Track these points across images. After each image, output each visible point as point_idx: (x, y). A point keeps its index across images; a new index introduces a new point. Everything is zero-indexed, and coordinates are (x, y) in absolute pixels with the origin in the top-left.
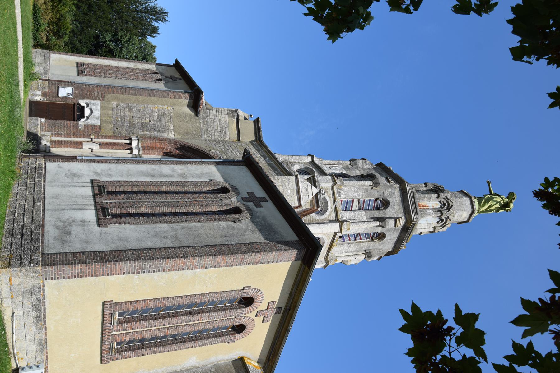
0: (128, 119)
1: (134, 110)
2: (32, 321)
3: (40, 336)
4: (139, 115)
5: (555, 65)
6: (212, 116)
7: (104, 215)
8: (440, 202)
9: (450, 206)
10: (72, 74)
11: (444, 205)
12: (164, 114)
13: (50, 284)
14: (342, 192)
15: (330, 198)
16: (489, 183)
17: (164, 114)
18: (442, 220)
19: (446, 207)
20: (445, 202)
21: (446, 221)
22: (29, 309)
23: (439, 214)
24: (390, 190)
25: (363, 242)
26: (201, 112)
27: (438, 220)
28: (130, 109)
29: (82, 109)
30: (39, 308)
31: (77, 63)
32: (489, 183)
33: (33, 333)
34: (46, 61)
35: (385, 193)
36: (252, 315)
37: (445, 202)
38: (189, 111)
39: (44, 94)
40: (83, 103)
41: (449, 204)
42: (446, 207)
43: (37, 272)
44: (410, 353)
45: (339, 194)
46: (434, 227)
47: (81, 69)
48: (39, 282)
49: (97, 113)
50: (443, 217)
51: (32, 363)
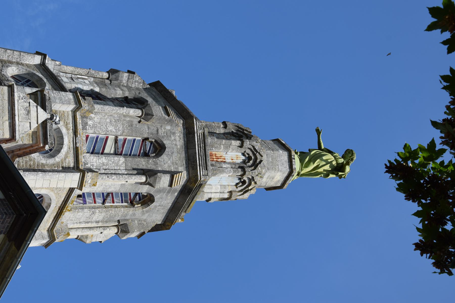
9: (258, 161)
11: (249, 158)
14: (90, 122)
15: (68, 129)
18: (244, 182)
20: (251, 154)
25: (116, 207)
37: (251, 154)
41: (256, 158)
45: (85, 125)
46: (231, 192)
50: (245, 178)
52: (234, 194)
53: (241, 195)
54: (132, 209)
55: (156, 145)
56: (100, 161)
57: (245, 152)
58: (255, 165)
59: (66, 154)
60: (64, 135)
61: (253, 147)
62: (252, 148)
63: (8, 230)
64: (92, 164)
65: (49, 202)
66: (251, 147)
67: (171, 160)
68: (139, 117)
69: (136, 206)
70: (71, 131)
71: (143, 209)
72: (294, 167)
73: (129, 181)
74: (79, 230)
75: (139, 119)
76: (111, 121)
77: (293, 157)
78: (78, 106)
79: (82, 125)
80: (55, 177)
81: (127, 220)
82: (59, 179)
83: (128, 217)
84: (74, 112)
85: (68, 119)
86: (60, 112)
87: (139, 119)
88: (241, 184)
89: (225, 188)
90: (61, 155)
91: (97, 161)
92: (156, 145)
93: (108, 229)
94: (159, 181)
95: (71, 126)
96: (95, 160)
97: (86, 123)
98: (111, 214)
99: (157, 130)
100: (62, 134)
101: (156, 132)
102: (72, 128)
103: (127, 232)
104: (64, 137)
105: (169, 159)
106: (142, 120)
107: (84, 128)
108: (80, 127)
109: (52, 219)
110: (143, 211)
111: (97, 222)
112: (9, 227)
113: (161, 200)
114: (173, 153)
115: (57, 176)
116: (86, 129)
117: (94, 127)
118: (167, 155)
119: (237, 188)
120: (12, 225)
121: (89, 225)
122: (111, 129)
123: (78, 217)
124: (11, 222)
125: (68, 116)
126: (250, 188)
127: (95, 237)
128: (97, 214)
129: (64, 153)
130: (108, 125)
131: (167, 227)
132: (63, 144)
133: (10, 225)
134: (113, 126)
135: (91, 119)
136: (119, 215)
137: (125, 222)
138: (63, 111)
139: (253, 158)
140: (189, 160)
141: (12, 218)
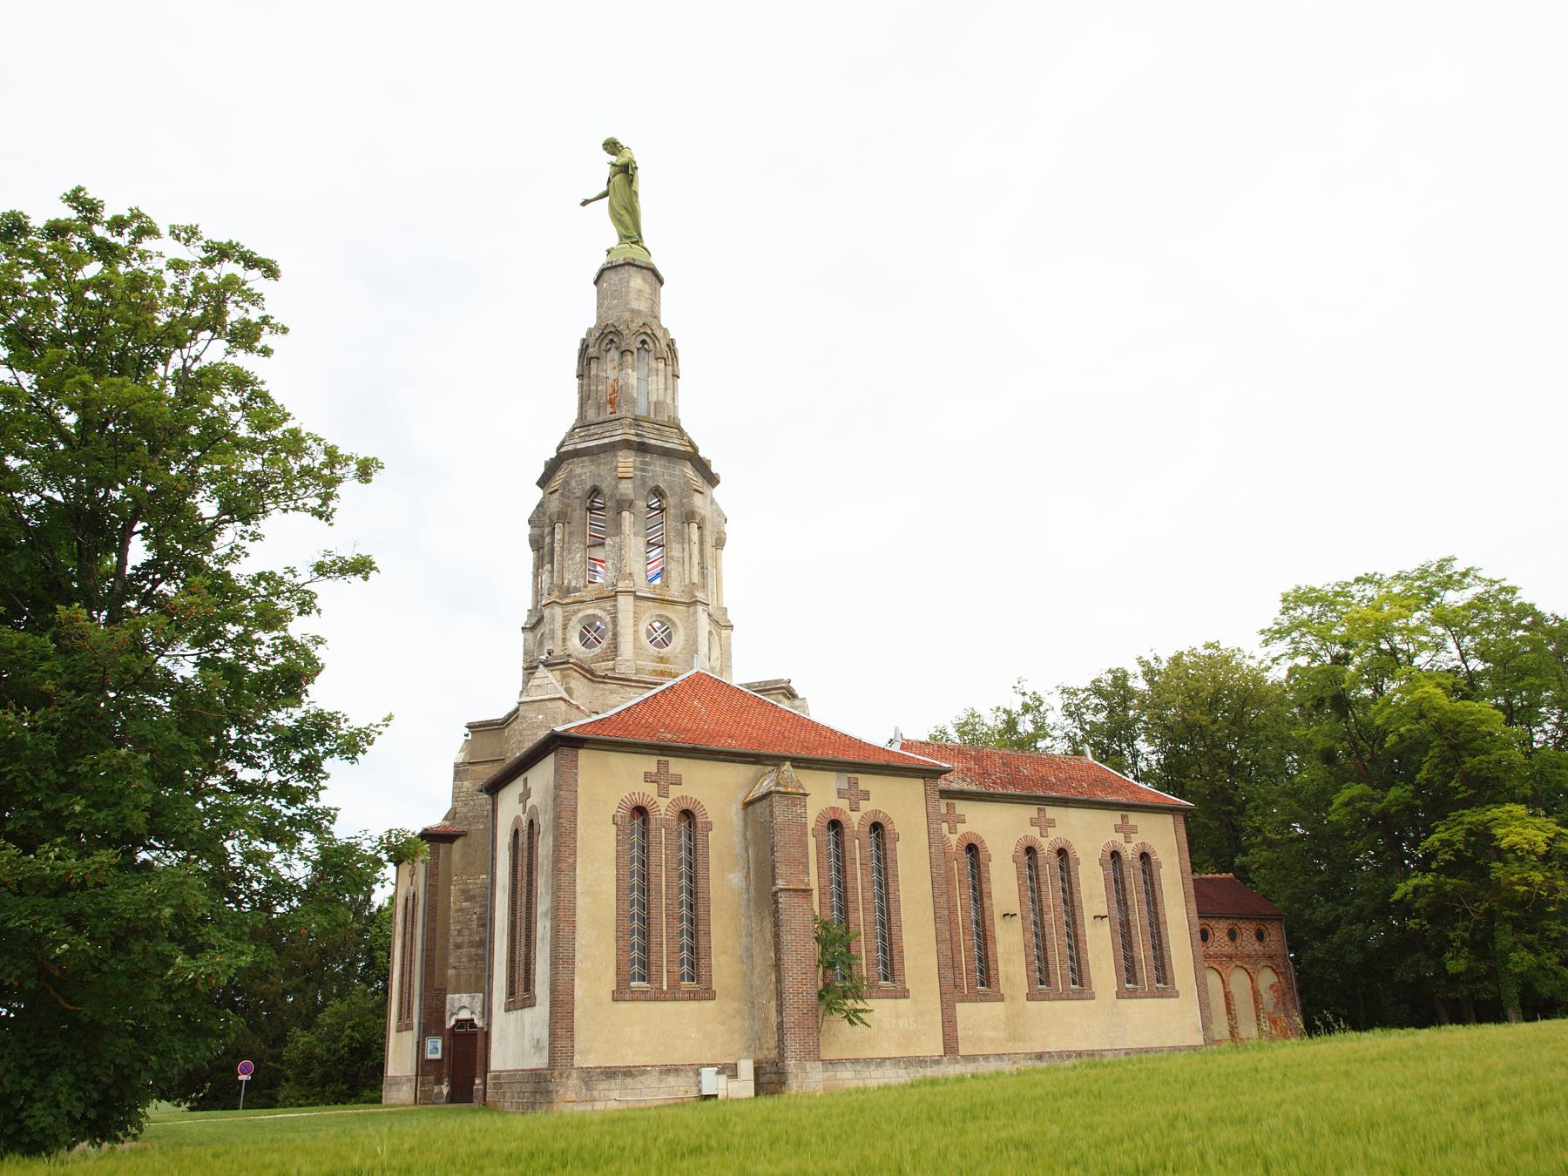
0: (473, 950)
1: (459, 940)
2: (629, 1080)
3: (655, 1074)
4: (466, 932)
5: (276, 545)
6: (465, 810)
7: (529, 1002)
10: (410, 1038)
11: (612, 341)
12: (464, 891)
13: (579, 1061)
16: (585, 203)
17: (464, 891)
22: (613, 1084)
26: (459, 828)
28: (458, 946)
29: (460, 1023)
30: (610, 1073)
31: (507, 1010)
32: (585, 203)
33: (651, 1080)
34: (397, 1081)
36: (663, 804)
38: (458, 844)
39: (439, 1082)
40: (450, 1023)
43: (561, 1075)
47: (404, 1027)
48: (574, 1074)
49: (465, 999)
51: (693, 1080)
95: (576, 607)
107: (577, 590)
117: (577, 578)
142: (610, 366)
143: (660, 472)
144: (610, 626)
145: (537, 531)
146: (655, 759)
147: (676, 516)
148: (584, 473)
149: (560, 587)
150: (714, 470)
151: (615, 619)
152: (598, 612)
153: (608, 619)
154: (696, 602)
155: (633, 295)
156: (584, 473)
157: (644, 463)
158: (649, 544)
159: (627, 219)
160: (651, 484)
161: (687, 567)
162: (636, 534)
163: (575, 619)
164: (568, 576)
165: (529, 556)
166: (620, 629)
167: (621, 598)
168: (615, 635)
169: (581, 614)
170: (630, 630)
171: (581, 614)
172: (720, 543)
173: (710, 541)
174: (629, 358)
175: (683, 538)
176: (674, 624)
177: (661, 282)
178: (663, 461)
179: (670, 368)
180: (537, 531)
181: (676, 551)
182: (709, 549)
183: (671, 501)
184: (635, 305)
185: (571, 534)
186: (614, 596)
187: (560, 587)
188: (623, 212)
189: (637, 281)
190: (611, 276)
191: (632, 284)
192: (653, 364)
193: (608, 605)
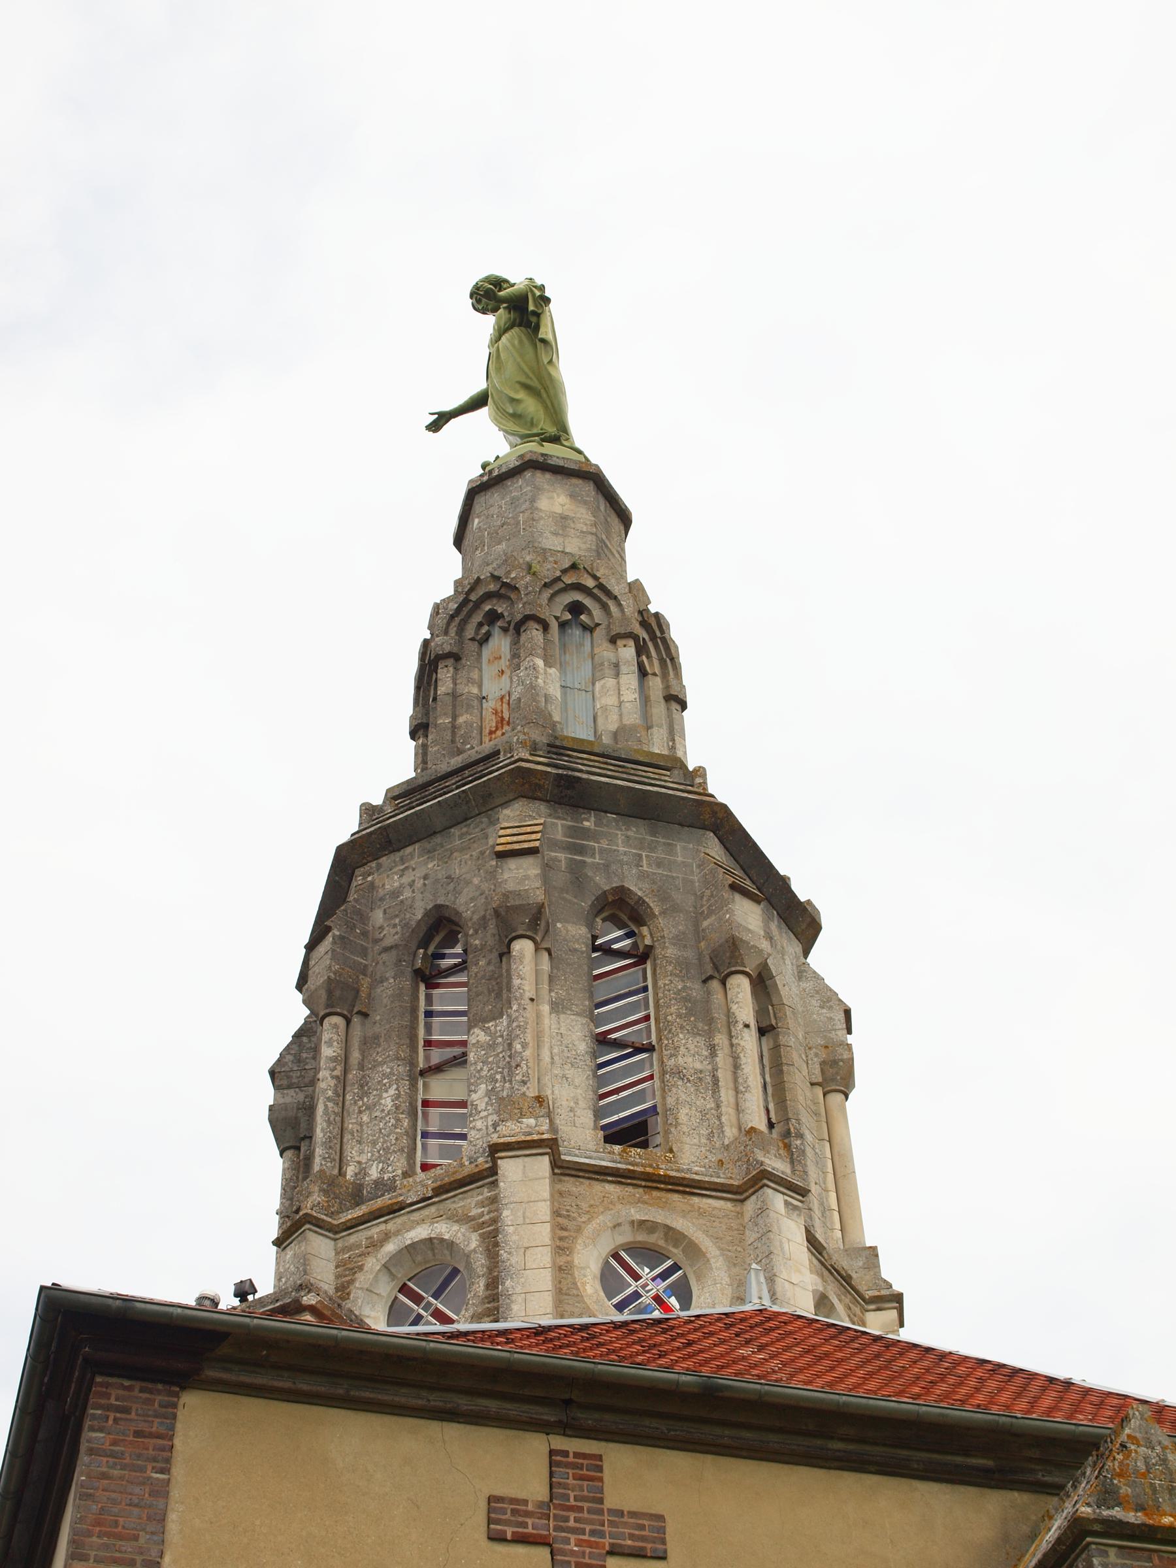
8: (487, 638)
9: (492, 587)
11: (493, 617)
14: (374, 1173)
15: (386, 1237)
16: (439, 422)
18: (576, 609)
19: (587, 602)
20: (478, 617)
21: (578, 587)
23: (534, 634)
24: (378, 917)
25: (657, 1006)
27: (577, 632)
32: (439, 422)
35: (388, 942)
37: (478, 617)
41: (488, 596)
42: (587, 602)
44: (368, 811)
45: (382, 1186)
46: (613, 640)
50: (557, 610)
52: (617, 629)
53: (620, 605)
54: (658, 951)
55: (437, 939)
56: (482, 1106)
57: (472, 639)
58: (506, 590)
59: (457, 1221)
60: (402, 1246)
61: (452, 617)
62: (457, 620)
63: (160, 1386)
64: (491, 1129)
65: (626, 1228)
66: (453, 624)
67: (468, 876)
68: (348, 1022)
69: (648, 942)
70: (391, 1226)
71: (654, 916)
72: (517, 463)
73: (528, 995)
74: (743, 1105)
75: (356, 1020)
76: (368, 1108)
77: (496, 473)
78: (307, 1226)
79: (383, 1195)
80: (515, 1238)
81: (700, 956)
82: (520, 1221)
83: (690, 954)
84: (336, 1233)
85: (359, 1246)
86: (337, 1277)
87: (356, 1020)
88: (582, 617)
89: (602, 664)
90: (459, 1234)
91: (484, 1114)
92: (437, 939)
93: (734, 1007)
94: (518, 894)
95: (375, 1230)
96: (479, 1124)
97: (378, 1183)
98: (679, 1016)
99: (387, 949)
100: (400, 1251)
101: (394, 952)
102: (383, 1227)
103: (734, 944)
104: (409, 1242)
105: (468, 883)
106: (355, 1010)
107: (390, 1186)
108: (385, 1200)
109: (696, 1199)
110: (663, 913)
111: (713, 1049)
112: (144, 1384)
113: (614, 867)
114: (449, 877)
115: (511, 1229)
116: (393, 1180)
117: (384, 1159)
118: (457, 892)
119: (598, 625)
120: (136, 1379)
121: (724, 1076)
122: (389, 1100)
123: (695, 1121)
124: (127, 1383)
125: (349, 1248)
126: (590, 583)
127: (833, 1035)
128: (681, 1060)
129: (456, 1227)
130: (378, 1114)
131: (720, 815)
132: (431, 1239)
133: (138, 1385)
134: (381, 1097)
135: (362, 1172)
136: (685, 988)
137: (707, 959)
138: (337, 1267)
139: (487, 608)
140: (466, 819)
141: (107, 1385)
142: (489, 671)
143: (625, 855)
144: (480, 1262)
145: (293, 1097)
146: (533, 1451)
147: (683, 966)
148: (408, 885)
149: (331, 1185)
150: (802, 891)
151: (492, 1239)
152: (445, 1230)
153: (473, 1242)
154: (760, 1179)
155: (545, 526)
156: (408, 885)
157: (585, 833)
158: (603, 1041)
159: (530, 406)
160: (603, 883)
161: (727, 1095)
162: (557, 1007)
163: (372, 1264)
164: (353, 1152)
165: (267, 1166)
166: (511, 1257)
167: (511, 1169)
168: (493, 1283)
169: (390, 1247)
170: (542, 1257)
171: (390, 1247)
172: (837, 1076)
173: (801, 1074)
174: (534, 634)
175: (707, 1020)
176: (693, 1250)
177: (625, 518)
178: (637, 831)
179: (656, 685)
180: (293, 1097)
181: (688, 1053)
182: (802, 1094)
183: (666, 931)
184: (551, 542)
185: (369, 1043)
186: (488, 1175)
187: (331, 1185)
188: (521, 395)
189: (556, 499)
190: (495, 500)
191: (543, 504)
192: (605, 652)
193: (471, 1202)
